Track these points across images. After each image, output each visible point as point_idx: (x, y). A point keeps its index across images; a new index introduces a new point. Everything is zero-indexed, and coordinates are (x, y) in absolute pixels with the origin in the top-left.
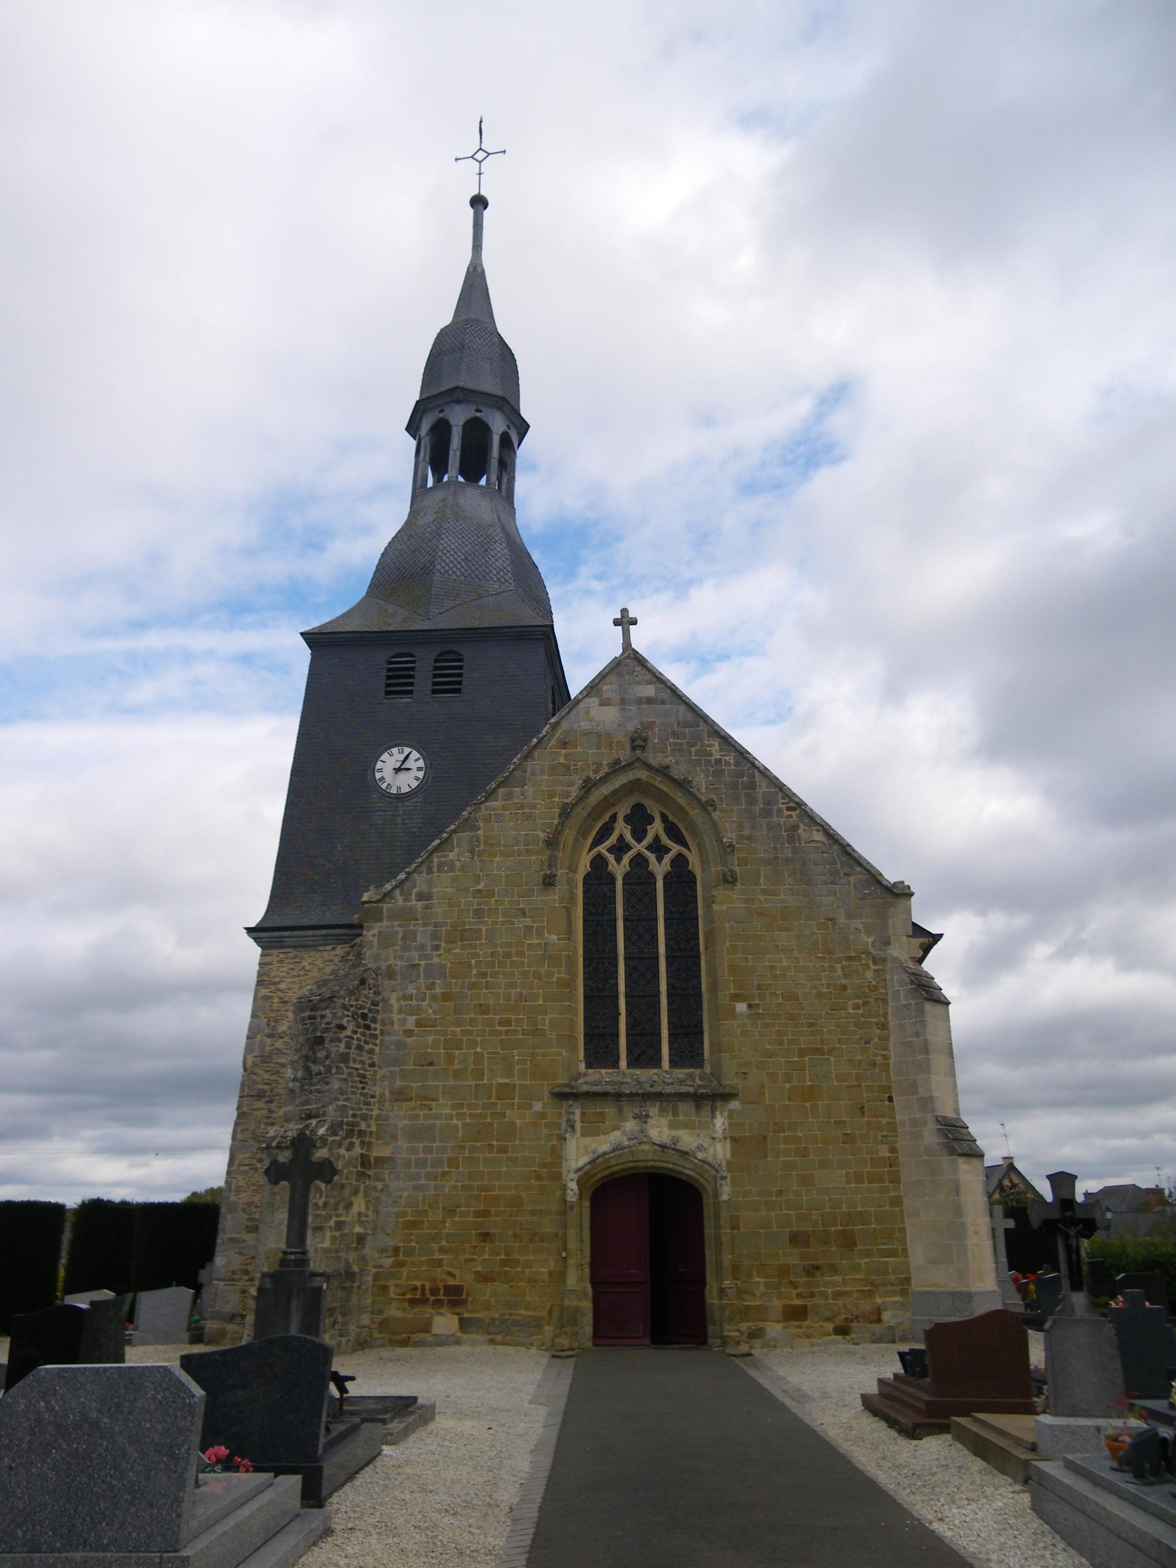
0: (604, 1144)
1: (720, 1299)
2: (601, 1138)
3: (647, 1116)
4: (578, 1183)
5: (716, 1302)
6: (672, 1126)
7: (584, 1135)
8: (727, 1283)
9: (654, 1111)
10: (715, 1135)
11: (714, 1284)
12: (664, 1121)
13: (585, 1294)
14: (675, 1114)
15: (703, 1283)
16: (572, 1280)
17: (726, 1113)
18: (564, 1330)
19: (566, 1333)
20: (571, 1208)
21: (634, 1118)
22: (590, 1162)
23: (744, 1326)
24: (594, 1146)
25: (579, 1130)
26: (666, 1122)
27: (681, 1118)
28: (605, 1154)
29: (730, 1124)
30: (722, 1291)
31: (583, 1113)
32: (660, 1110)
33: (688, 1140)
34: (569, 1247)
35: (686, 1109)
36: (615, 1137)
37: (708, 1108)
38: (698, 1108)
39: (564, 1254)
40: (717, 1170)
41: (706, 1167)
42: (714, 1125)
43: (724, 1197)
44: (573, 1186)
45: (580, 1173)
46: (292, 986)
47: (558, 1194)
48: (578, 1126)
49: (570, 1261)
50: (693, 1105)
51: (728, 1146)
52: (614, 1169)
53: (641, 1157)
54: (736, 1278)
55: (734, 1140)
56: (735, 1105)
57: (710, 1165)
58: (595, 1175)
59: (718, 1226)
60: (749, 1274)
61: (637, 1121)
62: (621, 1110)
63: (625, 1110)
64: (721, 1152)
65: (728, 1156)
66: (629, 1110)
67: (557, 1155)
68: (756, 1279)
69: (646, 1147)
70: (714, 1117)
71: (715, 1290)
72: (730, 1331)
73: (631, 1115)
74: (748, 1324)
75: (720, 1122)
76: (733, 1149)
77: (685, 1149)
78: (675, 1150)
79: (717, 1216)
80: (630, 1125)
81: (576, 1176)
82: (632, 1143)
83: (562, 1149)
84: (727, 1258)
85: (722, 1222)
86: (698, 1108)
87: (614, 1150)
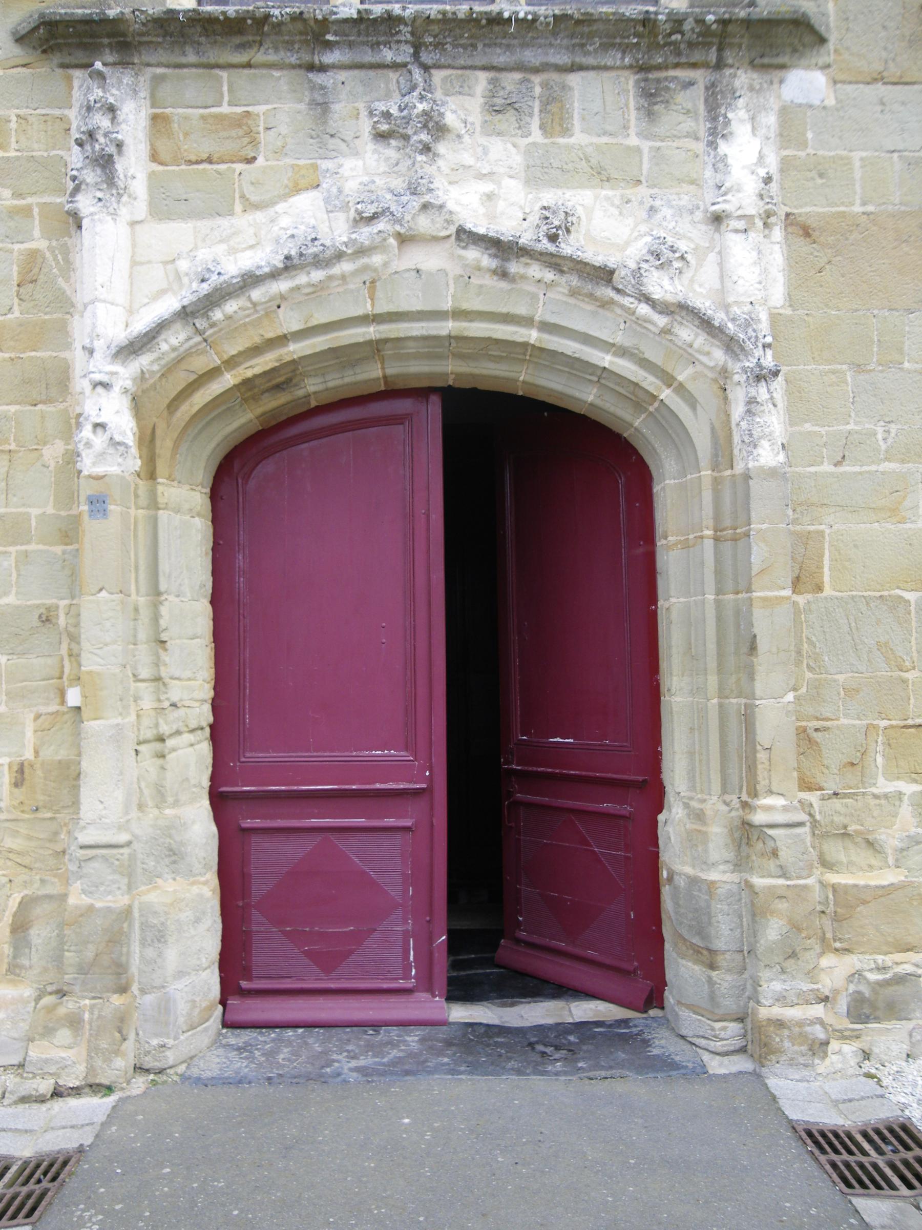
0: (243, 244)
1: (740, 864)
2: (244, 222)
3: (435, 127)
4: (137, 404)
5: (721, 876)
6: (538, 173)
7: (164, 206)
8: (772, 808)
9: (462, 104)
10: (728, 205)
11: (713, 805)
12: (505, 152)
13: (175, 856)
14: (556, 119)
15: (653, 793)
16: (106, 805)
17: (770, 120)
18: (69, 1005)
19: (74, 1022)
20: (98, 504)
21: (381, 137)
22: (185, 314)
23: (835, 971)
24: (204, 254)
25: (139, 187)
26: (517, 159)
27: (579, 138)
28: (250, 280)
29: (786, 165)
30: (747, 836)
31: (158, 122)
32: (494, 110)
33: (607, 229)
34: (90, 663)
35: (601, 97)
36: (305, 216)
37: (693, 99)
38: (652, 97)
39: (74, 697)
40: (732, 346)
41: (686, 333)
42: (721, 164)
43: (767, 456)
44: (115, 413)
45: (145, 361)
46: (757, 292)
47: (53, 452)
48: (134, 166)
49: (91, 726)
50: (630, 81)
51: (776, 256)
52: (296, 349)
53: (410, 299)
54: (806, 785)
55: (801, 229)
56: (805, 83)
57: (706, 324)
58: (213, 373)
59: (735, 577)
60: (855, 765)
61: (391, 151)
62: (321, 107)
63: (339, 108)
64: (751, 275)
65: (778, 295)
66: (357, 101)
67: (46, 284)
68: (884, 786)
69: (430, 259)
70: (717, 130)
71: (717, 831)
72: (780, 998)
73: (365, 126)
74: (852, 962)
75: (748, 151)
76: (796, 269)
77: (596, 256)
78: (555, 262)
79: (732, 534)
80: (364, 168)
81: (125, 374)
82: (365, 234)
83: (68, 267)
84: (775, 710)
85: (758, 554)
86: (652, 97)
87: (289, 266)
